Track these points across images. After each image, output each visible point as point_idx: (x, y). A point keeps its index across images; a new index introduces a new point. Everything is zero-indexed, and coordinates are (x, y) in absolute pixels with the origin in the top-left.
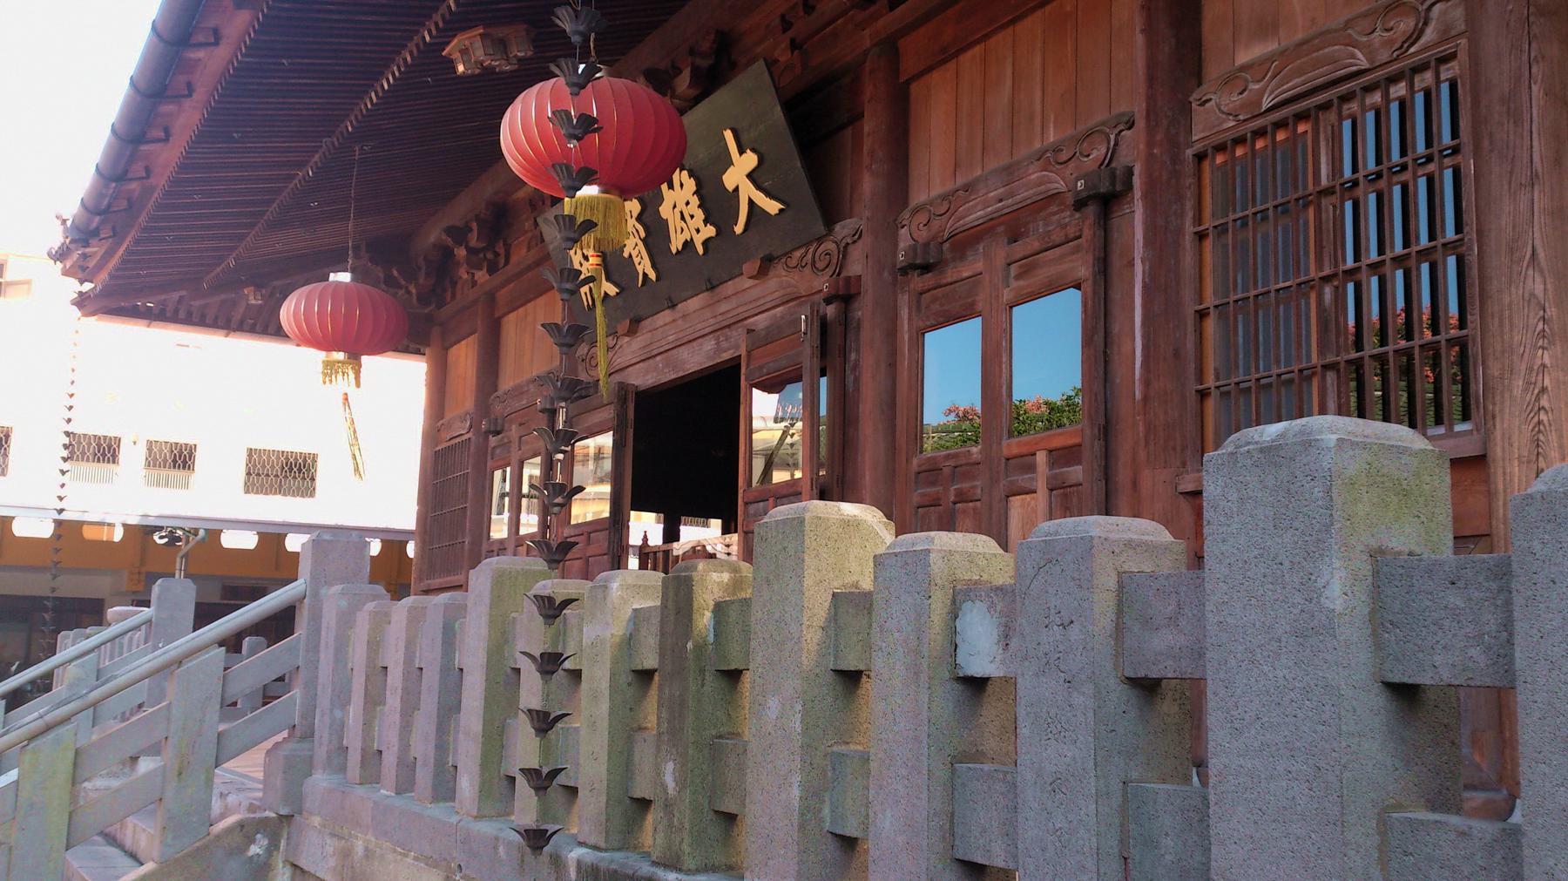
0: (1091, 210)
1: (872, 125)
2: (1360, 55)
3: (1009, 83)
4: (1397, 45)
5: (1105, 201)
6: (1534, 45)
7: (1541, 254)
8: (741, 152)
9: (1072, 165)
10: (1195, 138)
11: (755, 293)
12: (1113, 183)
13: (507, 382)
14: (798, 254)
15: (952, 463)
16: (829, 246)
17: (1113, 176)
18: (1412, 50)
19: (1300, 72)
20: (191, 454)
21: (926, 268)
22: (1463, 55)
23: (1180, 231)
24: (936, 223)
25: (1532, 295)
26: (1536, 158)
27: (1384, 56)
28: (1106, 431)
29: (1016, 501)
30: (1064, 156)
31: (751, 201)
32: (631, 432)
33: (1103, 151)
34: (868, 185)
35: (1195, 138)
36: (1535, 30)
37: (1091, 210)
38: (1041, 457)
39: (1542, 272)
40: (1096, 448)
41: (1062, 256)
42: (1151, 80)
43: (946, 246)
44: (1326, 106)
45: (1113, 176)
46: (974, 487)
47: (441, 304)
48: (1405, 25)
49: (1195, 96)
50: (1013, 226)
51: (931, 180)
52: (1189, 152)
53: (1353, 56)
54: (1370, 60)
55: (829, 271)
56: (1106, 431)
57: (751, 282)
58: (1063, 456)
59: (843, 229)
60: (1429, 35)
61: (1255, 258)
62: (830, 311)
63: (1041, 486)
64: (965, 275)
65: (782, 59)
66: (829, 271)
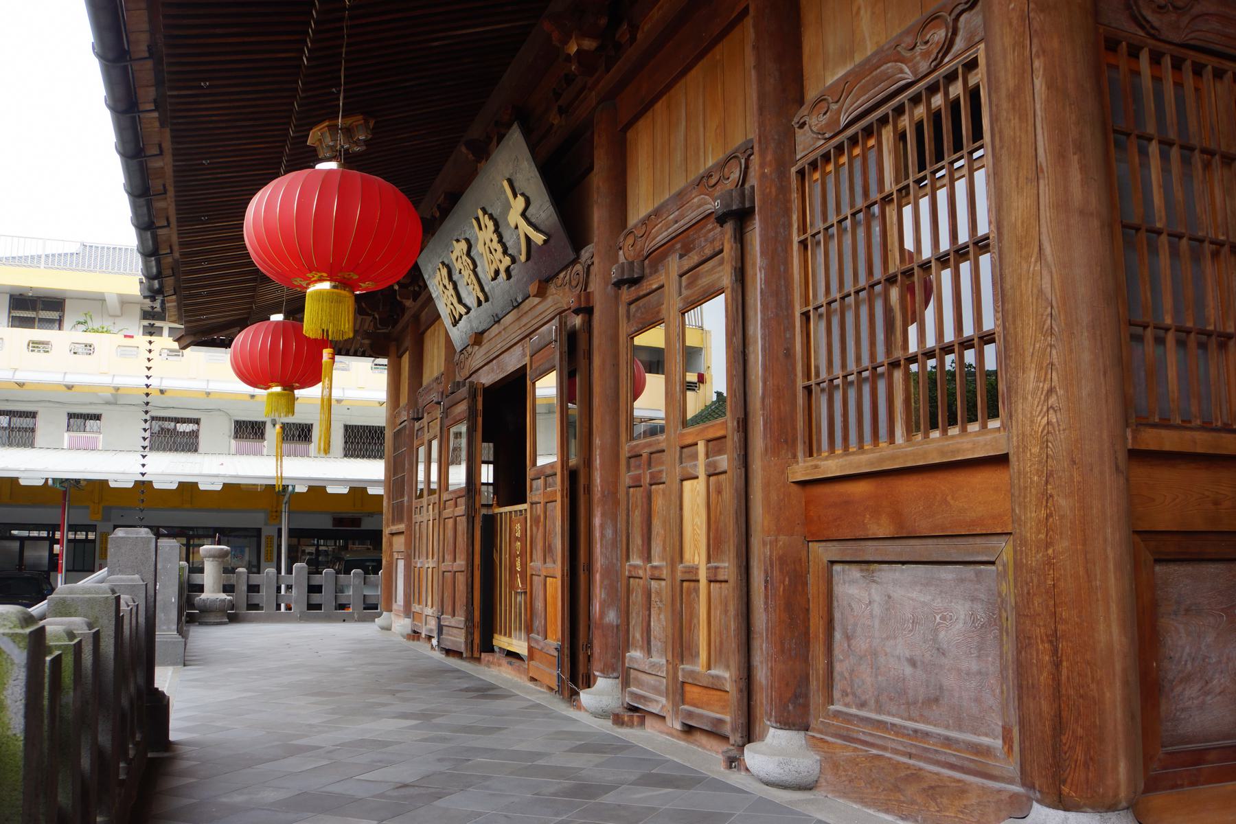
0: (729, 227)
1: (601, 164)
2: (907, 70)
3: (684, 123)
4: (933, 57)
5: (739, 217)
6: (1035, 41)
7: (1048, 249)
8: (515, 196)
9: (718, 187)
10: (798, 157)
11: (541, 308)
12: (743, 202)
13: (426, 380)
14: (562, 275)
15: (648, 450)
16: (578, 267)
17: (743, 195)
18: (947, 60)
19: (865, 90)
20: (236, 432)
21: (634, 282)
22: (982, 61)
23: (789, 241)
24: (640, 243)
25: (1041, 291)
26: (1041, 151)
27: (924, 67)
28: (744, 425)
29: (685, 483)
30: (713, 181)
31: (527, 237)
32: (480, 420)
33: (737, 174)
34: (599, 216)
35: (798, 157)
36: (1036, 25)
37: (729, 227)
38: (701, 447)
39: (1049, 266)
40: (736, 438)
41: (713, 268)
42: (761, 109)
43: (647, 262)
44: (883, 121)
45: (743, 195)
46: (661, 472)
47: (396, 322)
48: (939, 35)
49: (796, 120)
50: (683, 241)
51: (640, 208)
52: (794, 170)
53: (902, 71)
54: (914, 72)
55: (579, 288)
56: (744, 425)
57: (537, 300)
58: (716, 444)
59: (585, 254)
60: (959, 44)
61: (223, 228)
62: (577, 321)
63: (701, 472)
64: (654, 287)
65: (556, 122)
66: (579, 288)
